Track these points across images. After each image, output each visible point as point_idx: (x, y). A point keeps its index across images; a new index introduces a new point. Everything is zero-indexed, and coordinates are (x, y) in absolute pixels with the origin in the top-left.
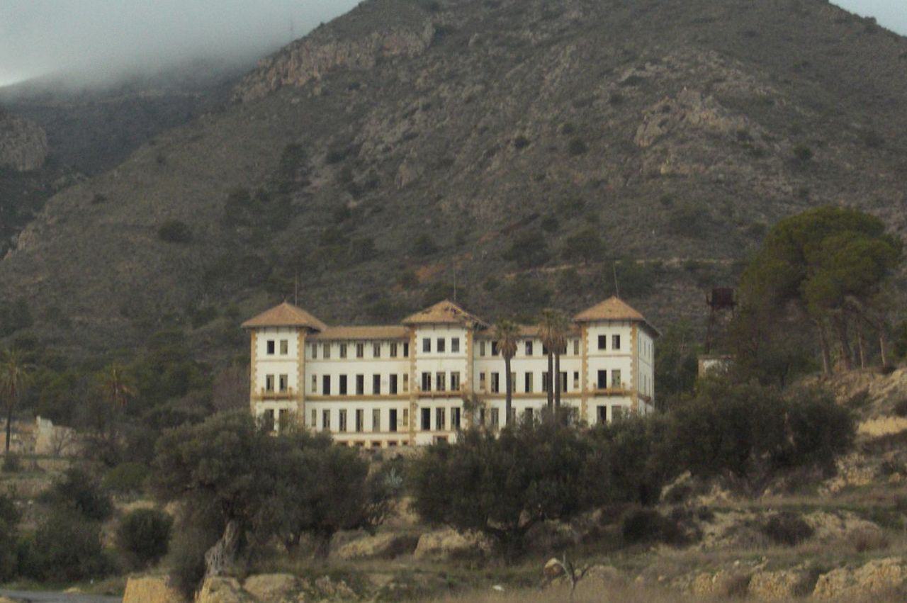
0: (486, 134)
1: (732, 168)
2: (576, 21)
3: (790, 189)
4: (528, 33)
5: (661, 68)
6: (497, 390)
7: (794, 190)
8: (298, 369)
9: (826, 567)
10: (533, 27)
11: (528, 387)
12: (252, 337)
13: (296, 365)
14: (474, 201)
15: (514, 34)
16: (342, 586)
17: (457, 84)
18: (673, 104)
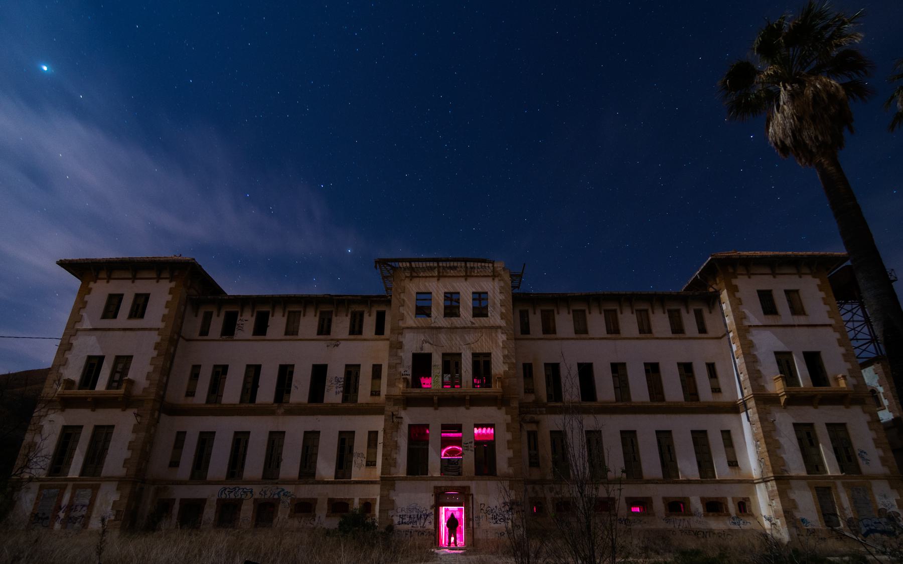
8: (157, 346)
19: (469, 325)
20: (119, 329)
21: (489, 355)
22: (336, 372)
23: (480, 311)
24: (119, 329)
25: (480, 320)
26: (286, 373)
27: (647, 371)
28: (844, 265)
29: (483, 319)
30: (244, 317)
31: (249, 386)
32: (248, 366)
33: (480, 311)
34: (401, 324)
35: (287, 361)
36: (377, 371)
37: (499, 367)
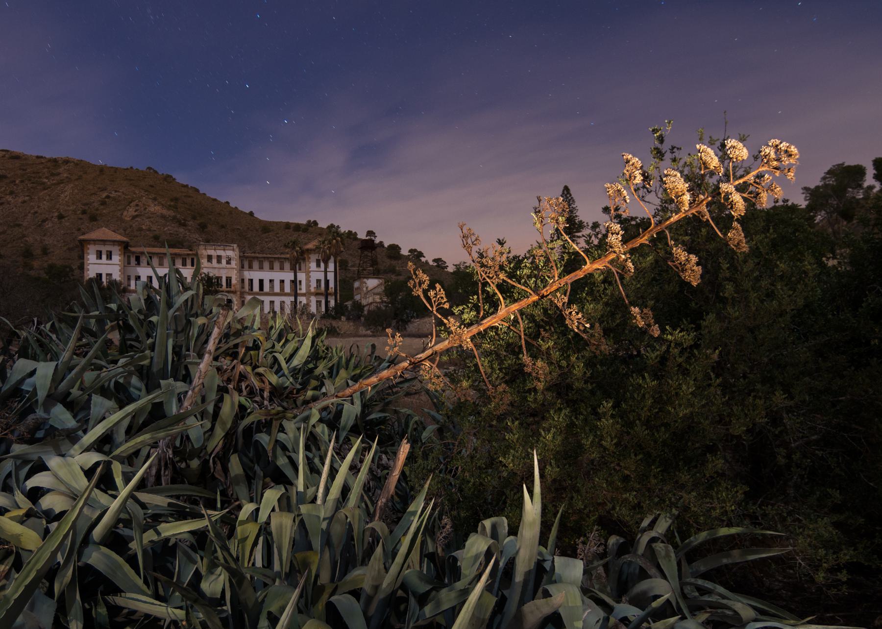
0: (36, 215)
1: (175, 229)
2: (67, 177)
5: (119, 194)
9: (270, 386)
10: (46, 178)
11: (251, 289)
12: (85, 252)
13: (118, 268)
14: (45, 238)
16: (87, 397)
17: (16, 196)
18: (140, 204)
21: (231, 277)
23: (228, 262)
27: (280, 282)
32: (148, 277)
33: (228, 262)
37: (234, 281)
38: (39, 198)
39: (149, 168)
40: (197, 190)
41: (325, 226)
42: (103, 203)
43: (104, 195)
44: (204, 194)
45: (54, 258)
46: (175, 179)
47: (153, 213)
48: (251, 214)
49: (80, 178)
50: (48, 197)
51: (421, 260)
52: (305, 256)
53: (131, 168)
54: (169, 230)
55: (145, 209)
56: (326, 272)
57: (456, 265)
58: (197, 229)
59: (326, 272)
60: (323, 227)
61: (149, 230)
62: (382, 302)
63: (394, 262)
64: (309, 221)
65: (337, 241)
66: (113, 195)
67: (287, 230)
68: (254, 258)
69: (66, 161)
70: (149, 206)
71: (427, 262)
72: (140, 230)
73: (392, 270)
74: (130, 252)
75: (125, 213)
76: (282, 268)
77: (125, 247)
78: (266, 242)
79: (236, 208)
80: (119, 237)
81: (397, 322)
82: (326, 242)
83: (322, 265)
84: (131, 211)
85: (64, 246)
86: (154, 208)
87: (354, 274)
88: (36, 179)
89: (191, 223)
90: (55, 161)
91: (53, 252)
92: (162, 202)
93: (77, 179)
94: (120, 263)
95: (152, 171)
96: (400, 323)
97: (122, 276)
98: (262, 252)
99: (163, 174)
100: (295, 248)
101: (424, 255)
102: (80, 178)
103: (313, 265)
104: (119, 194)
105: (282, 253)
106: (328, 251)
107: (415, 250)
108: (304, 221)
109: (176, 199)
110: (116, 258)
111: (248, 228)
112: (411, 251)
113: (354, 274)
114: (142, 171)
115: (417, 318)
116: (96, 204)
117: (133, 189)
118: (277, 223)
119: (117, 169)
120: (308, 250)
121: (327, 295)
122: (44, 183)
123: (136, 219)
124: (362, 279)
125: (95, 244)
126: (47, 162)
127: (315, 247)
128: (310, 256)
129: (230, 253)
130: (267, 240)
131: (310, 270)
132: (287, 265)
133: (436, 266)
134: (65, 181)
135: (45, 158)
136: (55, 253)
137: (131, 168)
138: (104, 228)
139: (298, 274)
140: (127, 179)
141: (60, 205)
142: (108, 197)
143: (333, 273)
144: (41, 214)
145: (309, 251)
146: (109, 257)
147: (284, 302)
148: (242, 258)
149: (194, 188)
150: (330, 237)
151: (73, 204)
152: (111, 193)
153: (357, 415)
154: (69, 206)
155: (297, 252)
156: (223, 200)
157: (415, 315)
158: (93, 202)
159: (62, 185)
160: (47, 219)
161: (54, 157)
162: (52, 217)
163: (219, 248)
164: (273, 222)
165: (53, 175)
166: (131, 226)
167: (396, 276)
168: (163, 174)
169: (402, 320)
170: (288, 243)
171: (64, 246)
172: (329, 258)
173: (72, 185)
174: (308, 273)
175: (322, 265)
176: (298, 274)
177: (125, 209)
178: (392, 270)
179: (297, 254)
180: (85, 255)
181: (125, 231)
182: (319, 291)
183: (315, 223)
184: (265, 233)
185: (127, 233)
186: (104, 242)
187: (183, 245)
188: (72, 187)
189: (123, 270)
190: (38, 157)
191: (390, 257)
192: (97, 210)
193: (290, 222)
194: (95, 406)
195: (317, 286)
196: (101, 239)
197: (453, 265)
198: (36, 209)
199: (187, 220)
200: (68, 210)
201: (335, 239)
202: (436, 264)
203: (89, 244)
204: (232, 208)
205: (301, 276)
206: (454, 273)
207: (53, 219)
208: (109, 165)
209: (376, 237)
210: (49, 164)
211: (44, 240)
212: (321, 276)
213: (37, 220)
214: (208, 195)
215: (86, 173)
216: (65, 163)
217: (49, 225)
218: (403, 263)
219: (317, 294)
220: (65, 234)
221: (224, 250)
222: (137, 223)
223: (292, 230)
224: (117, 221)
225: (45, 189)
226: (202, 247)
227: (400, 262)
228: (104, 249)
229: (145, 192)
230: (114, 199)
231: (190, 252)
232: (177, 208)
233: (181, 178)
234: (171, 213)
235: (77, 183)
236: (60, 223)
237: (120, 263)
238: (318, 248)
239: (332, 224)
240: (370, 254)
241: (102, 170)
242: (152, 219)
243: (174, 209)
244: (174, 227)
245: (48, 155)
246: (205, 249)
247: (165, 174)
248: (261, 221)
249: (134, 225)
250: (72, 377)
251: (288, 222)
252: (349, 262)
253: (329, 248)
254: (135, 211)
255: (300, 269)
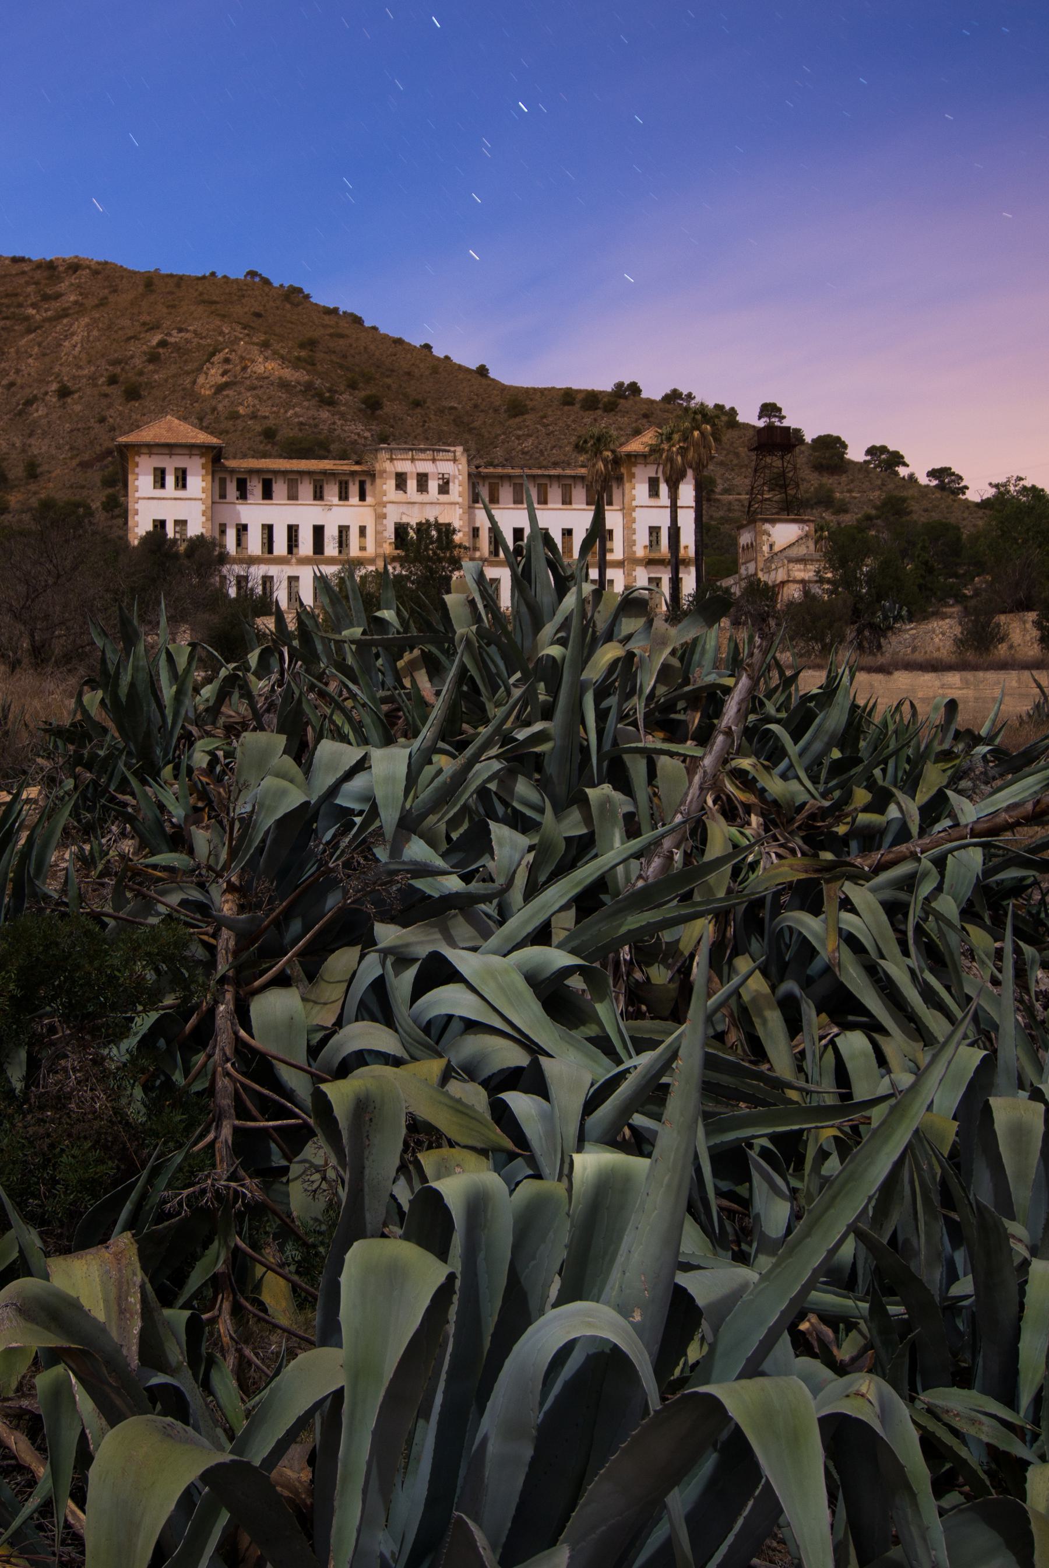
0: (13, 389)
1: (311, 413)
2: (76, 302)
3: (367, 434)
4: (32, 311)
5: (188, 335)
6: (270, 551)
7: (372, 435)
8: (204, 514)
10: (34, 305)
13: (200, 507)
14: (32, 441)
15: (17, 311)
18: (233, 356)
19: (435, 501)
20: (171, 499)
22: (331, 533)
23: (444, 489)
24: (171, 499)
25: (975, 676)
26: (293, 531)
27: (563, 534)
28: (468, 1521)
29: (446, 496)
30: (253, 484)
31: (266, 541)
32: (263, 525)
33: (444, 489)
34: (385, 499)
35: (319, 523)
36: (362, 531)
38: (17, 352)
39: (252, 274)
40: (357, 320)
41: (657, 396)
42: (153, 358)
43: (156, 339)
44: (375, 329)
45: (51, 485)
46: (307, 297)
47: (261, 378)
48: (482, 371)
49: (103, 303)
50: (36, 349)
51: (897, 474)
52: (623, 470)
53: (213, 274)
54: (296, 415)
55: (244, 369)
56: (674, 508)
57: (997, 486)
58: (360, 410)
59: (674, 508)
60: (653, 398)
61: (254, 416)
62: (821, 581)
63: (828, 481)
64: (620, 385)
65: (702, 434)
66: (175, 338)
67: (566, 408)
68: (502, 477)
69: (75, 267)
70: (253, 361)
71: (911, 476)
72: (234, 416)
73: (825, 501)
74: (225, 469)
75: (201, 380)
76: (567, 500)
77: (214, 458)
78: (518, 438)
79: (447, 358)
80: (203, 438)
81: (860, 632)
82: (676, 437)
83: (664, 489)
84: (214, 375)
85: (71, 458)
86: (265, 366)
87: (729, 510)
88: (12, 310)
89: (345, 397)
90: (50, 266)
91: (49, 472)
92: (282, 352)
93: (97, 306)
94: (203, 496)
95: (257, 279)
96: (867, 633)
97: (209, 525)
98: (508, 461)
99: (282, 286)
100: (601, 453)
101: (906, 460)
102: (103, 303)
103: (641, 491)
104: (188, 335)
105: (555, 465)
106: (679, 458)
107: (883, 449)
108: (605, 384)
109: (311, 344)
110: (197, 483)
111: (476, 406)
112: (872, 451)
113: (729, 510)
114: (237, 281)
115: (911, 621)
116: (137, 362)
117: (218, 323)
118: (542, 391)
119: (181, 278)
120: (629, 455)
121: (676, 563)
122: (27, 318)
123: (225, 393)
124: (759, 524)
125: (150, 454)
126: (33, 270)
127: (647, 449)
128: (634, 470)
129: (446, 467)
130: (520, 433)
131: (634, 503)
132: (579, 493)
133: (936, 486)
134: (71, 311)
135: (30, 260)
136: (54, 475)
137: (213, 274)
138: (169, 417)
139: (539, 514)
140: (204, 302)
141: (61, 365)
142: (163, 344)
143: (669, 510)
144: (22, 387)
145: (633, 458)
146: (181, 482)
147: (297, 578)
148: (474, 479)
149: (352, 315)
150: (687, 424)
151: (89, 362)
152: (170, 335)
153: (978, 876)
154: (80, 367)
155: (605, 461)
156: (416, 341)
157: (904, 613)
158: (132, 357)
159: (65, 321)
160: (35, 398)
161: (48, 259)
162: (46, 393)
163: (422, 456)
164: (534, 389)
165: (46, 298)
166: (214, 409)
167: (834, 514)
168: (282, 286)
169: (872, 627)
170: (586, 442)
171: (71, 458)
172: (682, 476)
173: (87, 320)
174: (628, 511)
175: (664, 489)
176: (538, 513)
177: (199, 369)
178: (825, 501)
179: (606, 466)
180: (131, 477)
181: (201, 419)
182: (655, 555)
183: (634, 388)
184: (515, 416)
185: (204, 424)
186: (170, 449)
187: (329, 451)
188: (87, 325)
189: (209, 513)
190: (15, 260)
191: (819, 468)
192: (141, 373)
193: (575, 387)
194: (500, 845)
195: (651, 541)
196: (163, 441)
197: (990, 484)
198: (12, 376)
199: (336, 392)
200: (79, 376)
201: (698, 428)
202: (935, 483)
203: (139, 454)
204: (438, 359)
205: (613, 520)
206: (985, 504)
207: (48, 398)
208: (165, 271)
209: (784, 417)
210: (38, 275)
211: (30, 446)
212: (664, 521)
213: (14, 400)
214: (383, 330)
215: (115, 291)
216: (70, 272)
217: (39, 411)
218: (852, 481)
219: (650, 562)
220: (72, 431)
221: (434, 460)
222: (226, 402)
223: (578, 406)
224: (183, 398)
225: (29, 331)
226: (383, 455)
227: (844, 478)
228: (170, 465)
229: (245, 328)
230: (177, 347)
231: (357, 468)
232: (314, 365)
233: (323, 297)
234: (300, 376)
235: (97, 315)
236: (64, 406)
237: (203, 496)
238: (655, 450)
239: (675, 391)
240: (778, 463)
241: (150, 282)
242: (259, 392)
243: (309, 367)
244: (308, 409)
245: (36, 254)
246: (391, 460)
247: (287, 285)
248: (504, 389)
249: (220, 407)
250: (445, 782)
251: (570, 389)
252: (719, 481)
253: (683, 451)
254: (223, 375)
255: (610, 503)
